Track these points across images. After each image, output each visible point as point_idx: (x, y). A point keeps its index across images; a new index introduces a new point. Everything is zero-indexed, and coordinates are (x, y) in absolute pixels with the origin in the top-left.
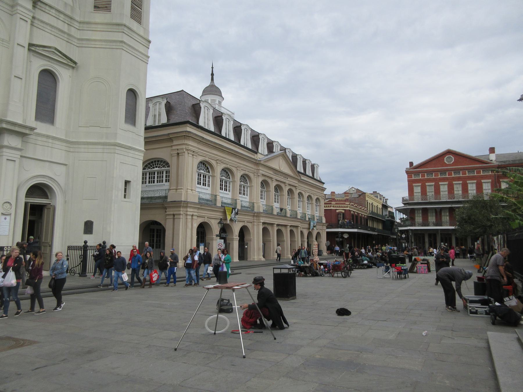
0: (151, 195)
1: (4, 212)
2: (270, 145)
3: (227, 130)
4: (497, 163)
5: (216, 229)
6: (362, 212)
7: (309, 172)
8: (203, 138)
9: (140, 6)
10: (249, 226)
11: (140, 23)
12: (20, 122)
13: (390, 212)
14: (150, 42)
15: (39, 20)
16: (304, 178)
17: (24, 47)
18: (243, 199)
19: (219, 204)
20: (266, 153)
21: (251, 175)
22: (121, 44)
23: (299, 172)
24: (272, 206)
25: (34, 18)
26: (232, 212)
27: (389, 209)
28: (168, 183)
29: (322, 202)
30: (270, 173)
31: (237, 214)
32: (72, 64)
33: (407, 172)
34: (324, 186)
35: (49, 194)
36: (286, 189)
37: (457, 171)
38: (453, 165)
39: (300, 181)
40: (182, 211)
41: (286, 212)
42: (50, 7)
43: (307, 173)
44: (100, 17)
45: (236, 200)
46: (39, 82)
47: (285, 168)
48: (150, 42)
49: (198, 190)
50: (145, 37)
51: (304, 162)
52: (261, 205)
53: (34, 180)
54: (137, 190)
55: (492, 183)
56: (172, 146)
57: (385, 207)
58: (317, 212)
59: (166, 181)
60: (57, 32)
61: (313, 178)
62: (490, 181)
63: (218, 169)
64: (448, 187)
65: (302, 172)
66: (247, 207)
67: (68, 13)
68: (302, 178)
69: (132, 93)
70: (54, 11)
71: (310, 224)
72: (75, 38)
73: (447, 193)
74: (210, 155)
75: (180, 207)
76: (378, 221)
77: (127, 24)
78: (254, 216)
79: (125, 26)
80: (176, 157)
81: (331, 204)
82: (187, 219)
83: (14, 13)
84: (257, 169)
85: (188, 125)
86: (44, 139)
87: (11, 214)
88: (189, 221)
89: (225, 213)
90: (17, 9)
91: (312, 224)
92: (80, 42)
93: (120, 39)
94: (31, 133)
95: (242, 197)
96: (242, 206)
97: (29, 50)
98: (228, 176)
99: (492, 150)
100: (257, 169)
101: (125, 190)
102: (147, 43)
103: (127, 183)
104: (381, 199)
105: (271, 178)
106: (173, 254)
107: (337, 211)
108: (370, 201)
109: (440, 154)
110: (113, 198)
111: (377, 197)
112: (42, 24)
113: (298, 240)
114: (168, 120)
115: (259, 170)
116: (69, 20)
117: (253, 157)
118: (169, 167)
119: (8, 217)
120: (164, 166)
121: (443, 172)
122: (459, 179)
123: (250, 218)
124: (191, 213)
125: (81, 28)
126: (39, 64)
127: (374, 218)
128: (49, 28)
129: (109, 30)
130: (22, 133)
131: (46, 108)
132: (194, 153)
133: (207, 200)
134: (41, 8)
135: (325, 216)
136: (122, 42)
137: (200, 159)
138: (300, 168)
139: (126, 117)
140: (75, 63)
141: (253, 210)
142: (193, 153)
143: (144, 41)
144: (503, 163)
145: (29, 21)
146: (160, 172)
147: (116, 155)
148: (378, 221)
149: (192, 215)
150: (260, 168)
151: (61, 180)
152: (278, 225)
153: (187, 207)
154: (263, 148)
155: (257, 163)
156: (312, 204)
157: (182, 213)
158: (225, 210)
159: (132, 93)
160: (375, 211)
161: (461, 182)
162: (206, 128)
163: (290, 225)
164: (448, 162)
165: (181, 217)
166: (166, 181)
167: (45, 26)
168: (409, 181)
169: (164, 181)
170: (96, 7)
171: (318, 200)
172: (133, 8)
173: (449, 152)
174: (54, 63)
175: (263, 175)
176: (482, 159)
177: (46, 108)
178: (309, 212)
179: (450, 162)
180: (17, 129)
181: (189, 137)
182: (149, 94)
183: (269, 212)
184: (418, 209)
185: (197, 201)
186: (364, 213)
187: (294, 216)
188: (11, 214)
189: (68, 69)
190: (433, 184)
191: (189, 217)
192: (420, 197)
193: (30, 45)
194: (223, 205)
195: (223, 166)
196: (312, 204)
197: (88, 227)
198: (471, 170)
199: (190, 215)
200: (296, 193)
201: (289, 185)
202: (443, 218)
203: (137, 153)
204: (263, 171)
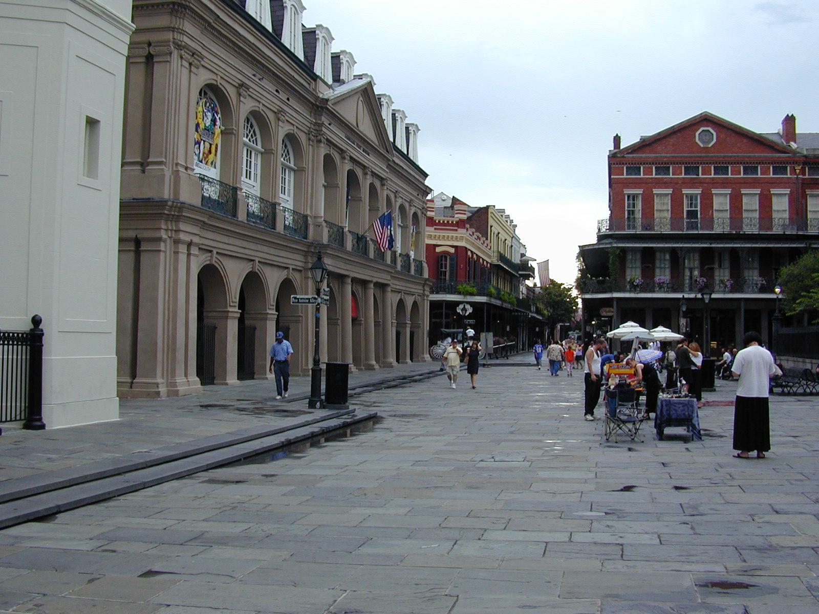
21: (303, 138)
34: (427, 182)
45: (274, 206)
49: (198, 170)
55: (791, 196)
62: (788, 191)
75: (160, 216)
80: (142, 67)
88: (183, 257)
103: (92, 123)
106: (374, 419)
107: (438, 250)
122: (724, 184)
132: (194, 59)
149: (190, 244)
153: (177, 219)
163: (375, 280)
164: (703, 142)
165: (162, 246)
173: (706, 119)
179: (709, 142)
184: (634, 250)
190: (670, 191)
191: (183, 249)
199: (183, 242)
202: (628, 272)
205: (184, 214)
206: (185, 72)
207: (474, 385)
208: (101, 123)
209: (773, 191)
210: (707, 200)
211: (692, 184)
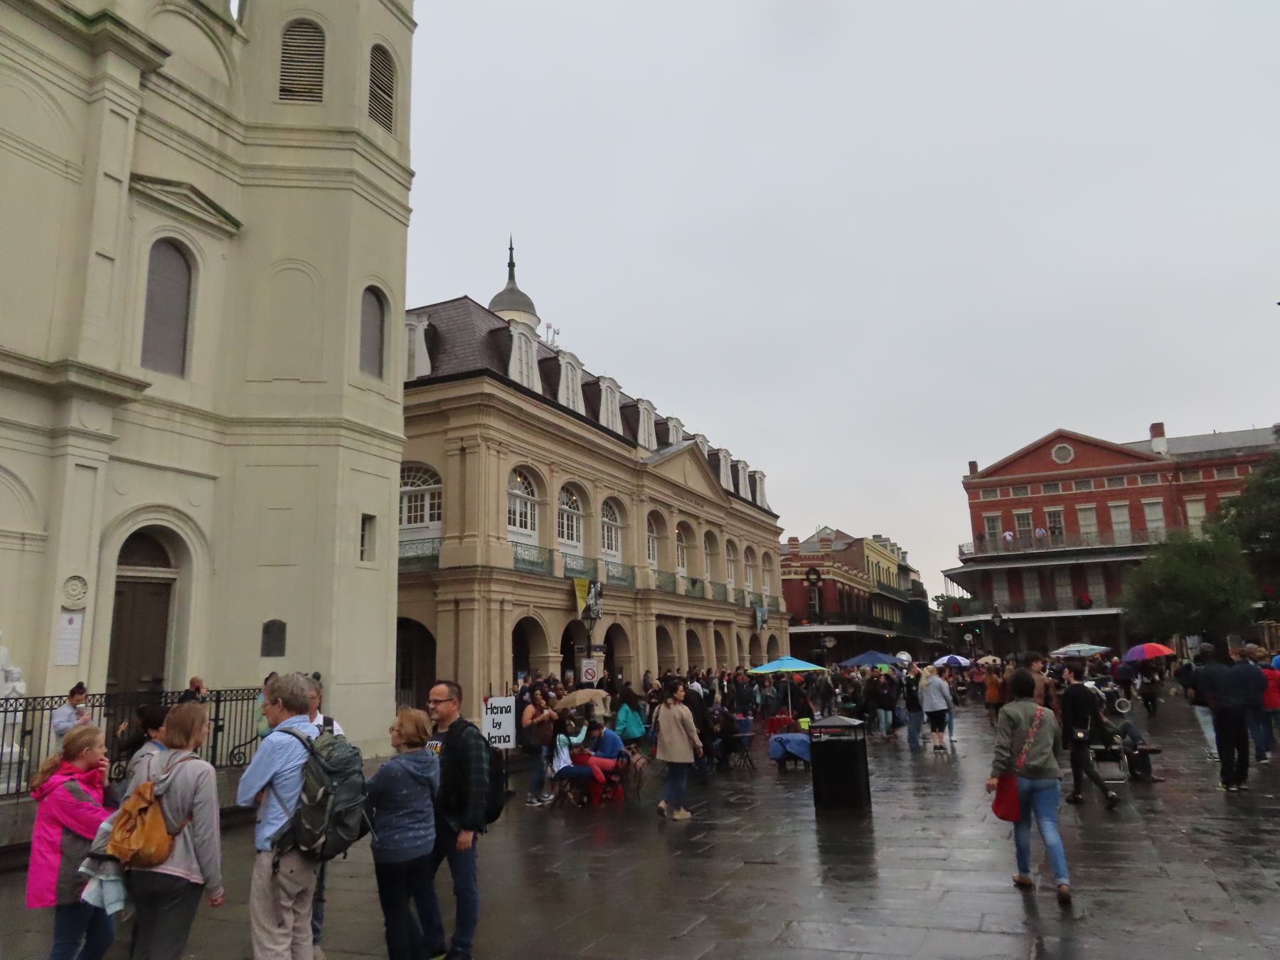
0: (410, 554)
1: (68, 604)
2: (662, 428)
3: (571, 395)
4: (1175, 459)
5: (554, 630)
6: (859, 583)
7: (745, 492)
8: (521, 410)
9: (388, 90)
10: (625, 623)
11: (388, 128)
12: (109, 367)
13: (914, 582)
14: (412, 174)
15: (153, 117)
16: (737, 505)
17: (120, 181)
18: (609, 559)
19: (559, 573)
20: (654, 446)
21: (625, 499)
22: (350, 178)
23: (727, 492)
24: (674, 575)
25: (142, 112)
26: (589, 592)
27: (913, 576)
28: (437, 524)
29: (777, 560)
30: (665, 494)
31: (600, 595)
32: (228, 225)
33: (968, 486)
34: (779, 523)
35: (171, 555)
36: (700, 532)
37: (1082, 480)
38: (1074, 464)
39: (732, 514)
40: (477, 591)
41: (703, 588)
42: (180, 87)
43: (742, 494)
44: (297, 114)
45: (595, 561)
46: (151, 272)
47: (697, 483)
48: (412, 174)
49: (511, 538)
50: (402, 162)
51: (735, 467)
52: (648, 577)
53: (151, 516)
54: (390, 542)
56: (446, 432)
57: (904, 570)
58: (767, 587)
59: (432, 518)
60: (194, 147)
61: (753, 504)
63: (555, 484)
64: (1130, 513)
65: (732, 490)
66: (619, 579)
67: (221, 103)
68: (734, 506)
69: (376, 296)
70: (186, 97)
71: (754, 617)
72: (236, 164)
73: (1128, 526)
74: (539, 451)
75: (472, 581)
76: (893, 604)
77: (364, 131)
78: (635, 600)
79: (358, 134)
80: (457, 459)
81: (789, 566)
82: (489, 610)
83: (95, 97)
84: (638, 486)
85: (487, 379)
86: (163, 413)
87: (84, 609)
89: (572, 594)
90: (104, 89)
91: (759, 615)
92: (249, 174)
93: (348, 167)
94: (139, 396)
95: (606, 554)
96: (608, 577)
97: (131, 190)
98: (574, 505)
99: (1157, 430)
100: (638, 486)
101: (363, 536)
102: (405, 176)
103: (367, 520)
104: (892, 551)
105: (669, 506)
108: (873, 558)
109: (1042, 440)
110: (337, 560)
111: (885, 546)
112: (160, 128)
113: (680, 657)
114: (433, 368)
115: (643, 486)
116: (222, 120)
117: (627, 455)
118: (438, 482)
119: (77, 618)
120: (424, 483)
121: (1051, 483)
122: (1088, 497)
123: (627, 606)
124: (500, 597)
125: (248, 141)
126: (154, 225)
127: (883, 598)
128: (174, 137)
129: (319, 145)
130: (113, 393)
131: (169, 338)
133: (532, 563)
134: (158, 90)
135: (787, 596)
136: (351, 172)
137: (515, 461)
138: (726, 482)
139: (363, 356)
140: (237, 224)
141: (633, 585)
142: (498, 448)
143: (400, 172)
144: (1187, 459)
145: (132, 119)
146: (416, 497)
147: (341, 449)
148: (893, 604)
149: (502, 602)
150: (646, 482)
151: (202, 517)
152: (689, 620)
154: (646, 435)
155: (639, 471)
156: (755, 567)
157: (477, 596)
158: (573, 586)
159: (376, 296)
160: (884, 580)
161: (1093, 505)
162: (525, 385)
163: (714, 619)
165: (476, 605)
166: (432, 518)
167: (166, 132)
168: (971, 506)
169: (427, 517)
170: (285, 91)
171: (767, 556)
172: (373, 96)
174: (187, 225)
175: (653, 500)
176: (1137, 448)
177: (169, 338)
178: (749, 587)
180: (103, 386)
181: (491, 407)
182: (411, 304)
183: (667, 590)
185: (511, 565)
186: (864, 584)
187: (721, 601)
188: (84, 609)
189: (220, 239)
191: (495, 606)
192: (1129, 533)
193: (135, 178)
194: (568, 574)
195: (565, 478)
196: (755, 567)
197: (274, 638)
198: (1114, 476)
199: (495, 601)
200: (722, 540)
201: (708, 522)
203: (388, 445)
204: (651, 488)
205: (495, 577)
206: (493, 459)
207: (66, 691)
208: (378, 518)
209: (1110, 504)
210: (1072, 516)
211: (1053, 501)
